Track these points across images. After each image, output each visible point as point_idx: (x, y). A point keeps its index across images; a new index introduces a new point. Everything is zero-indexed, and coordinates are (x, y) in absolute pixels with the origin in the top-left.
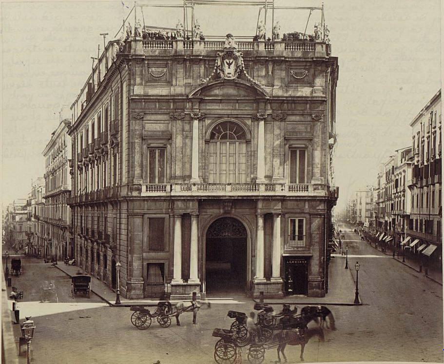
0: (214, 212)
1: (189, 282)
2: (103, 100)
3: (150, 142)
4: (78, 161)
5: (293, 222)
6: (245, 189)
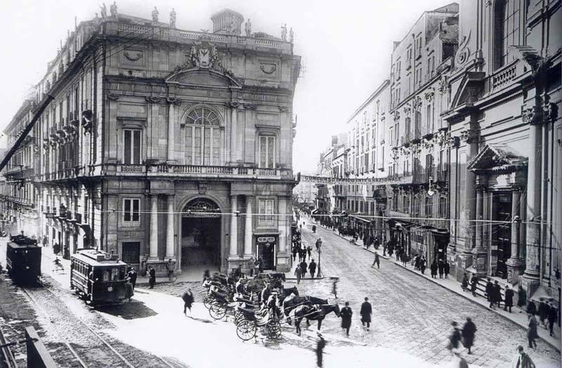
2: (73, 80)
3: (124, 122)
4: (45, 140)
5: (128, 203)
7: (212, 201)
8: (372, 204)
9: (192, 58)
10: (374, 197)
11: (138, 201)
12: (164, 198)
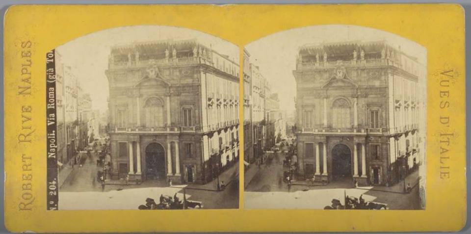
0: (147, 140)
1: (137, 173)
6: (348, 131)
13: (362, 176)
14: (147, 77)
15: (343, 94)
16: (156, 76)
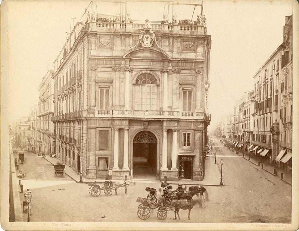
0: (138, 128)
5: (185, 134)
7: (151, 133)
8: (270, 136)
9: (139, 42)
10: (270, 132)
11: (190, 133)
12: (121, 130)
13: (172, 170)
14: (140, 46)
15: (151, 67)
16: (151, 45)
